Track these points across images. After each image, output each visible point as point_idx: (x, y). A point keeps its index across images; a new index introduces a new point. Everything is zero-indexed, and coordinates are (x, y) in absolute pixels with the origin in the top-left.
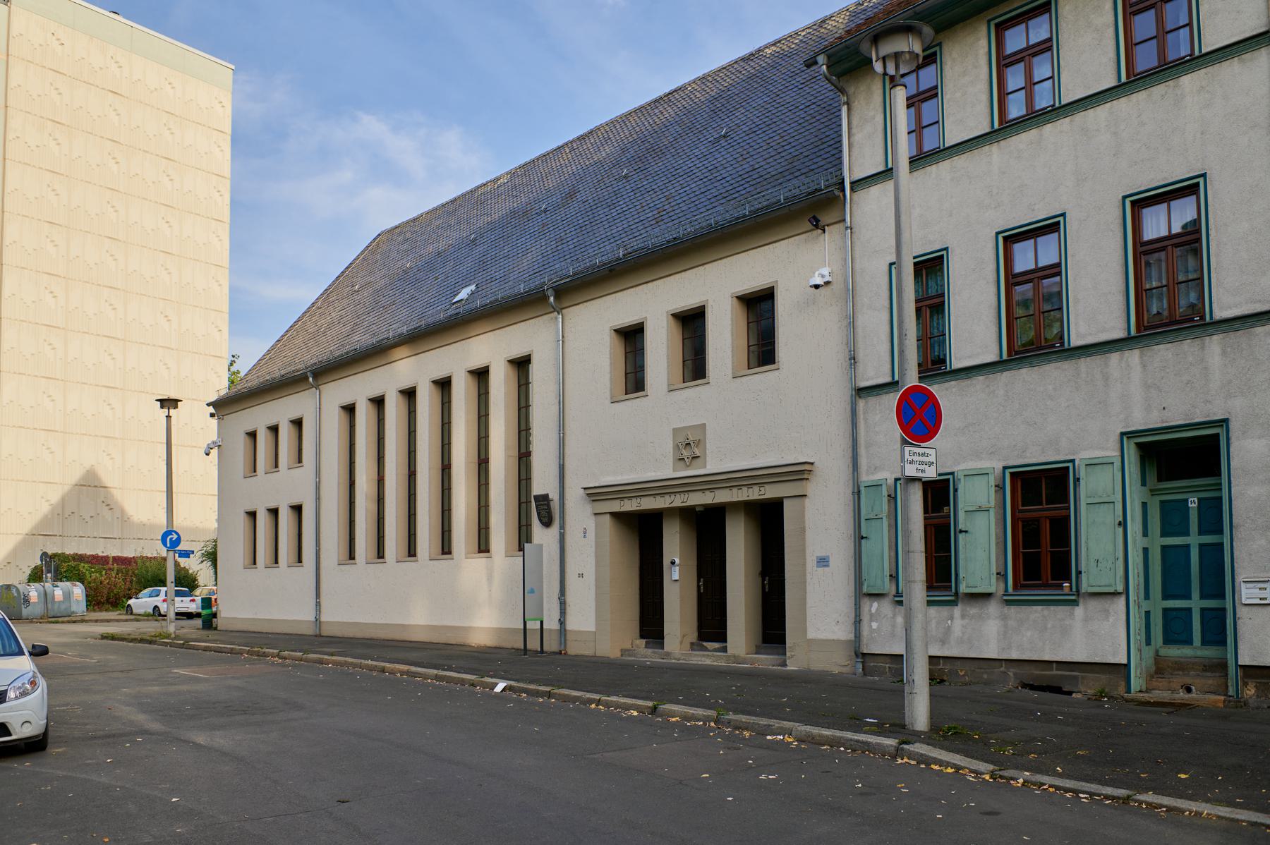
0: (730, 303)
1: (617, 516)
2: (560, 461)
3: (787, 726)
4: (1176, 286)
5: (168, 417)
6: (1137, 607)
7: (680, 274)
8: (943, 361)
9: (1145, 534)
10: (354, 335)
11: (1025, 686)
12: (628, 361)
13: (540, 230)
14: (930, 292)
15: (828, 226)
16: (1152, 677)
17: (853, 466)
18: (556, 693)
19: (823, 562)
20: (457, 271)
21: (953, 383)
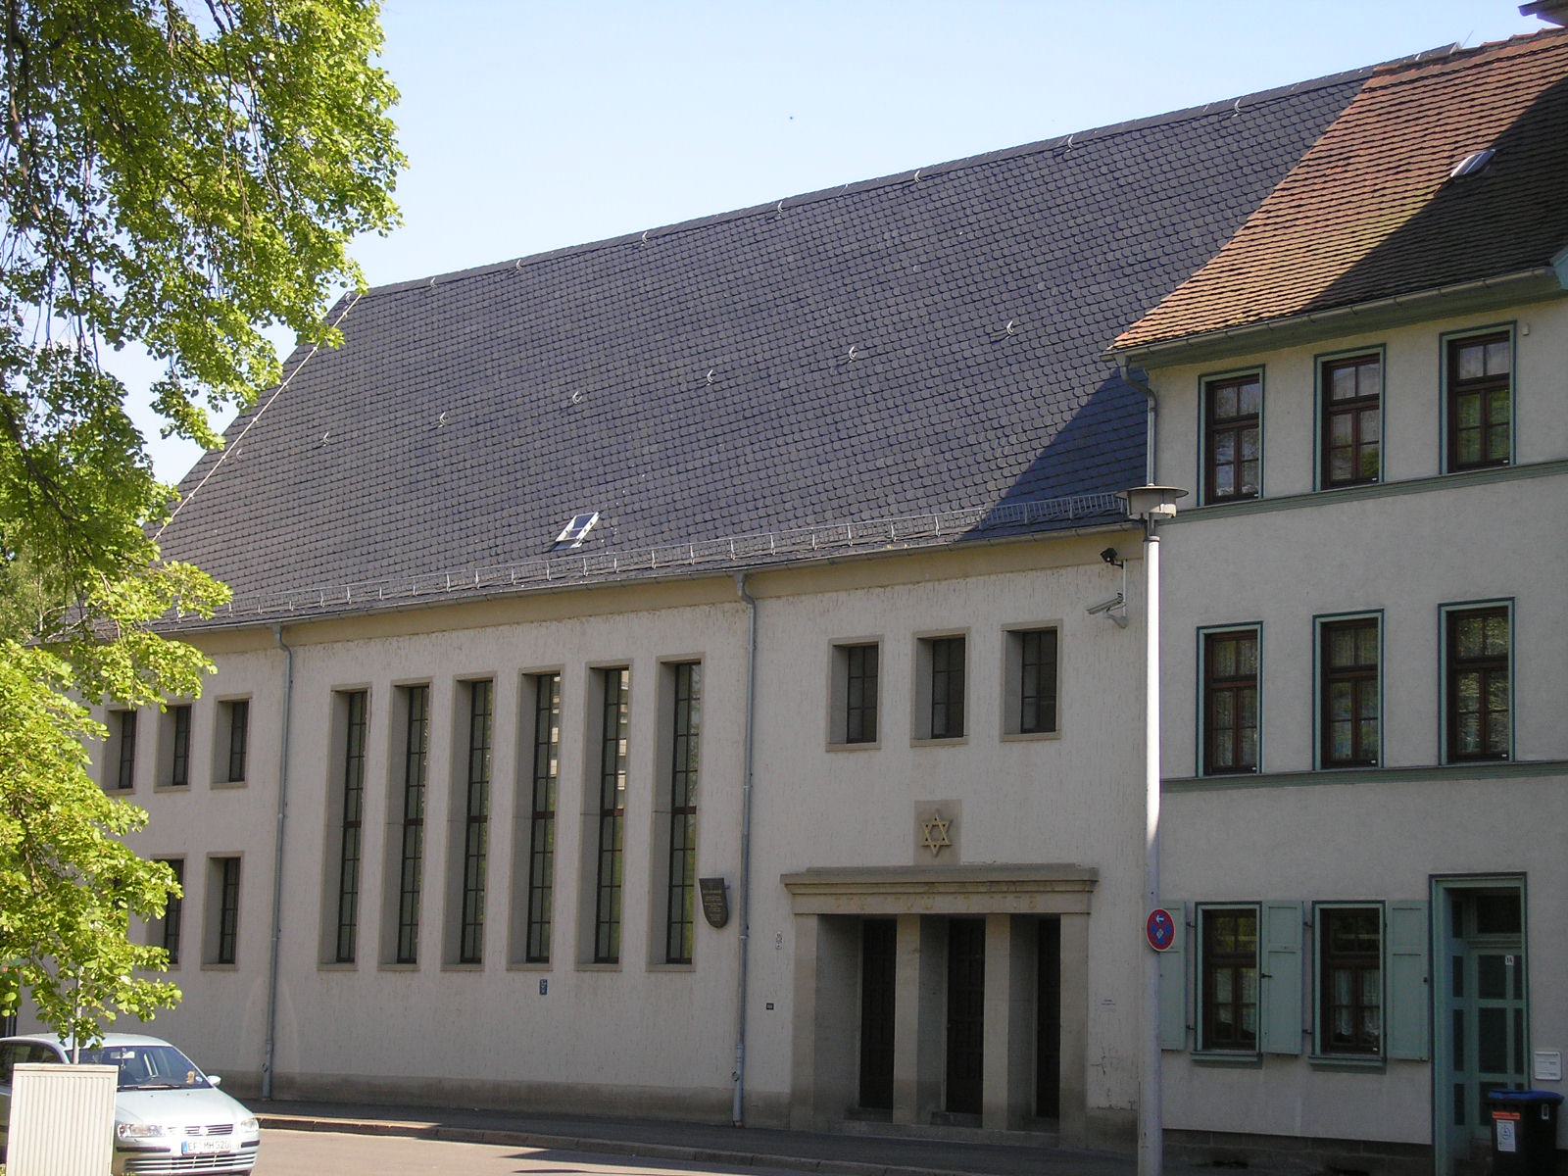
1: (832, 923)
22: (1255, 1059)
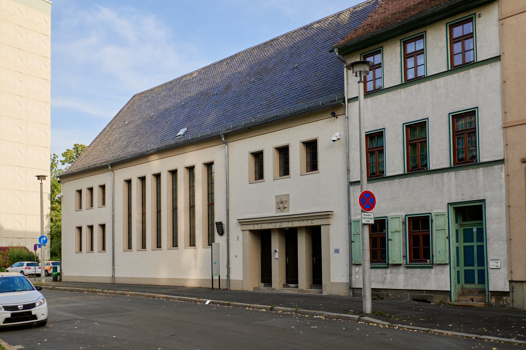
0: (299, 144)
1: (252, 232)
2: (227, 208)
3: (321, 313)
4: (468, 148)
5: (41, 184)
6: (454, 269)
7: (278, 131)
8: (383, 172)
9: (457, 241)
10: (129, 147)
11: (414, 300)
12: (256, 166)
13: (215, 104)
14: (378, 145)
15: (339, 116)
16: (460, 296)
17: (349, 213)
18: (231, 304)
19: (337, 251)
20: (177, 120)
21: (387, 181)
22: (387, 266)
